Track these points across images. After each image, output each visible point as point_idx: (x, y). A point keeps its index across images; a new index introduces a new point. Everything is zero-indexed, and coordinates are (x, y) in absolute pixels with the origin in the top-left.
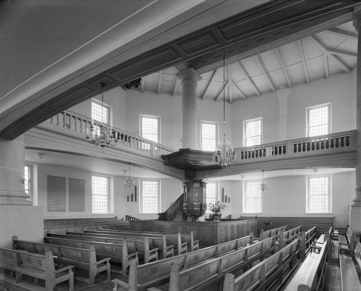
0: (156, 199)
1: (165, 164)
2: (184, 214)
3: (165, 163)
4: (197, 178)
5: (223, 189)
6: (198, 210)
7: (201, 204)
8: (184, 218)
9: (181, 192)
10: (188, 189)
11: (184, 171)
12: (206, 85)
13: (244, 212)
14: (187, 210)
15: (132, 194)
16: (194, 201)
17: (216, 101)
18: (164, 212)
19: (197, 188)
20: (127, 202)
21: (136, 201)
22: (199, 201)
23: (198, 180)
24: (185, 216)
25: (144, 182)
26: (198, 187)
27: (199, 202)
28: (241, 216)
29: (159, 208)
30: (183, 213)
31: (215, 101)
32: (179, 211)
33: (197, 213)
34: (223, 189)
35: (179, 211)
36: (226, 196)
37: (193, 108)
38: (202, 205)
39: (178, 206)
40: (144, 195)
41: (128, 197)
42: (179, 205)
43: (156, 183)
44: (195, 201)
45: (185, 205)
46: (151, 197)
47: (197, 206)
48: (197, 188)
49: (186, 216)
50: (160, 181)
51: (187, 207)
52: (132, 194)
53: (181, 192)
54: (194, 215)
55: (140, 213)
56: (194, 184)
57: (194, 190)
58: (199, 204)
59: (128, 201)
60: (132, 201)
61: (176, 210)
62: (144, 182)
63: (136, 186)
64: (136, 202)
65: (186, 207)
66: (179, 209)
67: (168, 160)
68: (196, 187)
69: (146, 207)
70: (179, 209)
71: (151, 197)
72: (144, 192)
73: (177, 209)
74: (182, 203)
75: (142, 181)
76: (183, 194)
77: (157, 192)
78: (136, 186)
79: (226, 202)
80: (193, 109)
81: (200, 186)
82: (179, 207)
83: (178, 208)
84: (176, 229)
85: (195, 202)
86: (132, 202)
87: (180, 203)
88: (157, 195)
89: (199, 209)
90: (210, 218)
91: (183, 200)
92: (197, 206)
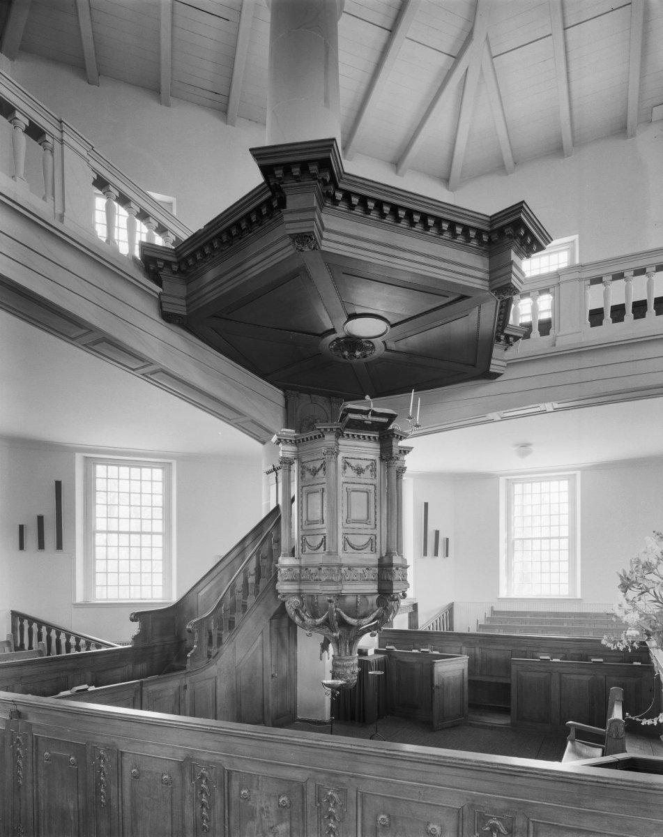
0: (158, 540)
1: (168, 317)
2: (282, 611)
3: (168, 308)
4: (368, 404)
5: (426, 505)
6: (364, 595)
7: (381, 559)
8: (280, 634)
9: (264, 503)
10: (308, 475)
11: (277, 395)
12: (363, 87)
13: (503, 593)
14: (299, 594)
15: (40, 519)
16: (341, 540)
17: (400, 171)
18: (175, 599)
19: (359, 471)
20: (21, 551)
21: (59, 546)
22: (372, 542)
23: (369, 419)
24: (285, 623)
25: (100, 470)
26: (364, 464)
27: (373, 550)
28: (495, 610)
29: (167, 573)
30: (275, 607)
31: (397, 172)
32: (250, 601)
33: (361, 612)
34: (426, 505)
35: (250, 601)
36: (437, 533)
37: (327, 47)
38: (391, 565)
39: (245, 571)
40: (100, 524)
41: (21, 527)
42: (253, 565)
43: (158, 473)
44: (347, 540)
45: (290, 568)
46: (145, 533)
47: (360, 571)
48: (359, 471)
49: (292, 626)
50: (174, 463)
51: (301, 575)
52: (40, 519)
53: (264, 503)
54: (343, 623)
55: (79, 599)
56: (341, 441)
57: (341, 479)
58: (372, 558)
59: (22, 547)
60: (41, 546)
61: (239, 596)
62: (100, 470)
63: (58, 485)
64: (59, 554)
65: (298, 580)
66: (251, 590)
67: (180, 289)
68: (353, 463)
69: (149, 570)
70: (251, 590)
71: (145, 533)
72: (100, 511)
73: (239, 587)
74: (273, 555)
75: (510, 483)
76: (277, 508)
77: (158, 513)
78: (58, 485)
79: (436, 554)
80: (326, 100)
81: (377, 458)
82: (251, 580)
83: (246, 583)
84: (228, 802)
85: (349, 549)
86: (42, 554)
87: (258, 553)
88: (158, 526)
89: (373, 588)
90: (410, 627)
91: (278, 541)
92: (360, 571)
